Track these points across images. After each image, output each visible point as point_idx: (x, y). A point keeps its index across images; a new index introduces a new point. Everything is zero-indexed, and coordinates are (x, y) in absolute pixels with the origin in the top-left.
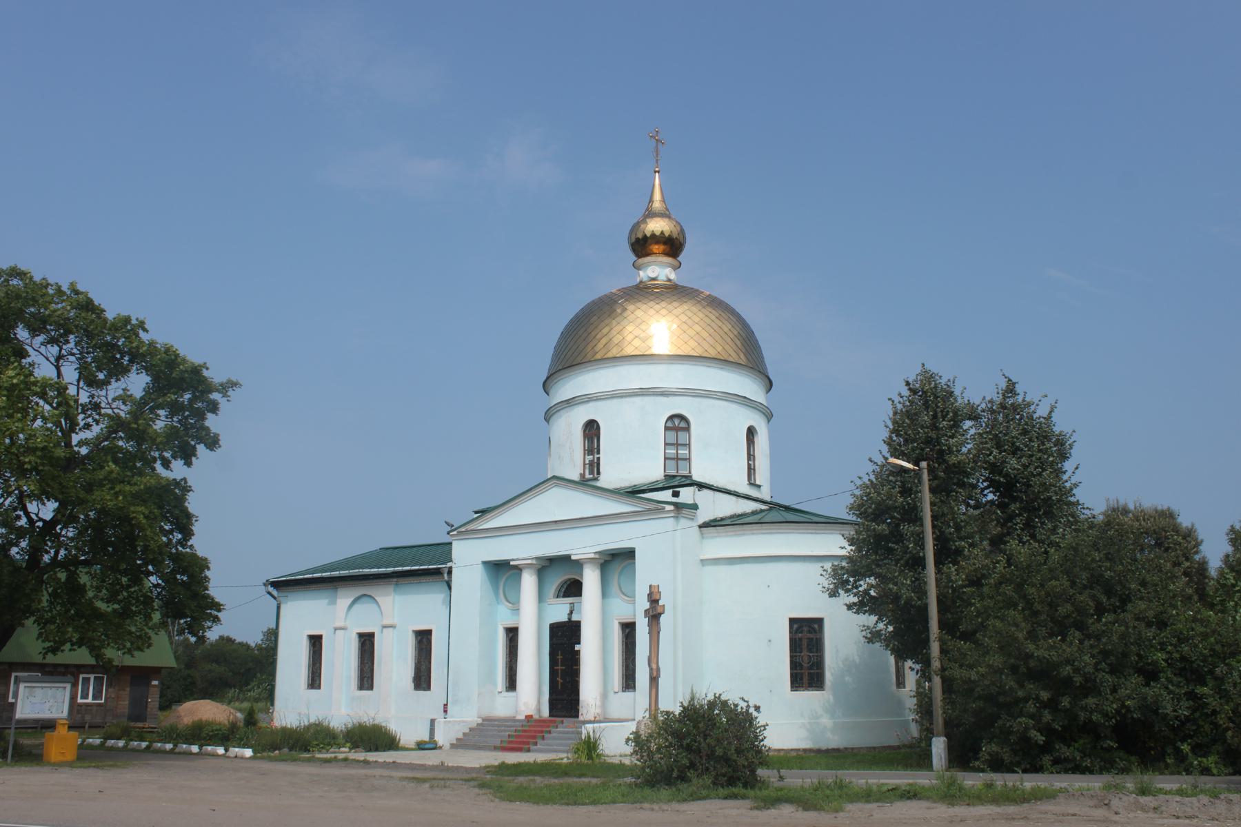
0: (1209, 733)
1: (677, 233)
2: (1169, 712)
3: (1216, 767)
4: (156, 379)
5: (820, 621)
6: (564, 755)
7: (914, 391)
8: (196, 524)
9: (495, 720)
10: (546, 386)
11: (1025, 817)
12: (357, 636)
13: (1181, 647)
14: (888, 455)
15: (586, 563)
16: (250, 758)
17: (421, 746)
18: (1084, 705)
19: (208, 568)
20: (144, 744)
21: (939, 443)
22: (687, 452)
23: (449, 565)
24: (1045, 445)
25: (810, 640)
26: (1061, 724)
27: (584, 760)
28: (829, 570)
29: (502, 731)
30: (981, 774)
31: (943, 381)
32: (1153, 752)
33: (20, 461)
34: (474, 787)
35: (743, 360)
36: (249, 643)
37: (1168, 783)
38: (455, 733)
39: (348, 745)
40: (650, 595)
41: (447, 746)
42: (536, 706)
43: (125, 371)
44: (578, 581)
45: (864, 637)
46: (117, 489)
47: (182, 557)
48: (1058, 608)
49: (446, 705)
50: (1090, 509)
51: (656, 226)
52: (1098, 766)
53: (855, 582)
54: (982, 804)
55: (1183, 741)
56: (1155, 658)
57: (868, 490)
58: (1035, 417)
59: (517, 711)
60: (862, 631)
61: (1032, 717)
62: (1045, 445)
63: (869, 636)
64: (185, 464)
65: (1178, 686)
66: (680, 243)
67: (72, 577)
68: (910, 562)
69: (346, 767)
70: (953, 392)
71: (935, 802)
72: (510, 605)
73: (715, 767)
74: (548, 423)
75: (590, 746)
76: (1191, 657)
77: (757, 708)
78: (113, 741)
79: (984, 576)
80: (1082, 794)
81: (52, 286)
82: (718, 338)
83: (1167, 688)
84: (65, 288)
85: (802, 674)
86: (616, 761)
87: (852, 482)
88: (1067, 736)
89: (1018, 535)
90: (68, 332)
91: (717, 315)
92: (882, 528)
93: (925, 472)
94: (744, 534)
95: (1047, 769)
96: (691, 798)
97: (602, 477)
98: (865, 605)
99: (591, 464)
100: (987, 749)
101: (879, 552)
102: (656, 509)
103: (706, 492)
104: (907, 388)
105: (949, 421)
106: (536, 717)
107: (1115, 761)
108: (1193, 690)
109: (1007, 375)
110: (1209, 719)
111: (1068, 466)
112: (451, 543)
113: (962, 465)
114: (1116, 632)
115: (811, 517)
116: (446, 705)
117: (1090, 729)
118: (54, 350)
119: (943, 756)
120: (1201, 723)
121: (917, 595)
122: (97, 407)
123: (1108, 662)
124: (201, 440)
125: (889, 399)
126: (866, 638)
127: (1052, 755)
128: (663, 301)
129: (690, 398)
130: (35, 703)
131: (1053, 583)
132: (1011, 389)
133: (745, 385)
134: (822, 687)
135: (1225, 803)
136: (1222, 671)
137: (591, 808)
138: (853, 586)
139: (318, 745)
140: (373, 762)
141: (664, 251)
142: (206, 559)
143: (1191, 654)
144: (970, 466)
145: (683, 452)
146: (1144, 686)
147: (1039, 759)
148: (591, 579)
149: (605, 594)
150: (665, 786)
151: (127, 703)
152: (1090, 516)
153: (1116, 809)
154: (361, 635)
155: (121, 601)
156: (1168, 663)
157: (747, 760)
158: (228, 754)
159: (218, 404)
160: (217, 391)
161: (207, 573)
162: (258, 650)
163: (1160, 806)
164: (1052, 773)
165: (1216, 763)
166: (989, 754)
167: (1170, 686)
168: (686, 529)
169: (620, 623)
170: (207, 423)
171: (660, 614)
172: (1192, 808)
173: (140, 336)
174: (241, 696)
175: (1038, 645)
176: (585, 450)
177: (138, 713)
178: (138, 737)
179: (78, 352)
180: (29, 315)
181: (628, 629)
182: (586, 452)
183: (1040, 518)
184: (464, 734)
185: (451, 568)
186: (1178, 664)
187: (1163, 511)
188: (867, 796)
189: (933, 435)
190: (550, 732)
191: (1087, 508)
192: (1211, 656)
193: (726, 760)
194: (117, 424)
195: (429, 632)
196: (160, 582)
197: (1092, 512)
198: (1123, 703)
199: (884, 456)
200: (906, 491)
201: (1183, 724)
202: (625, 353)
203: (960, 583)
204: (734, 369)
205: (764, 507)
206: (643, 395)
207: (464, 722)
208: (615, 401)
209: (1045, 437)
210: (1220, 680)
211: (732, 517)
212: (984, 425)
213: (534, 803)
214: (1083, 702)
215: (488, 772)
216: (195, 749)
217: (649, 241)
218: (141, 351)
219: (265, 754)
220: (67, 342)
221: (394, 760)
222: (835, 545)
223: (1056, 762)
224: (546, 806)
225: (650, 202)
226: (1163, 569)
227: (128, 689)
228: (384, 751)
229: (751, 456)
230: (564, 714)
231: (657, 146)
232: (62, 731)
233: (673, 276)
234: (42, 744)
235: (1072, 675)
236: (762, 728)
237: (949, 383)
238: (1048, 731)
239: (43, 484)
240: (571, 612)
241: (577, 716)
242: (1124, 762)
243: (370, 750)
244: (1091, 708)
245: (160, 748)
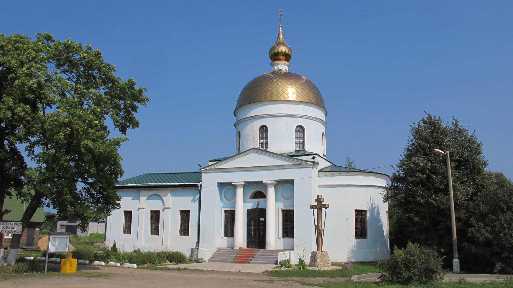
16: (137, 268)
41: (207, 261)
51: (283, 49)
103: (319, 157)
148: (271, 192)
169: (281, 210)
182: (260, 138)
185: (201, 184)
195: (188, 212)
240: (258, 205)
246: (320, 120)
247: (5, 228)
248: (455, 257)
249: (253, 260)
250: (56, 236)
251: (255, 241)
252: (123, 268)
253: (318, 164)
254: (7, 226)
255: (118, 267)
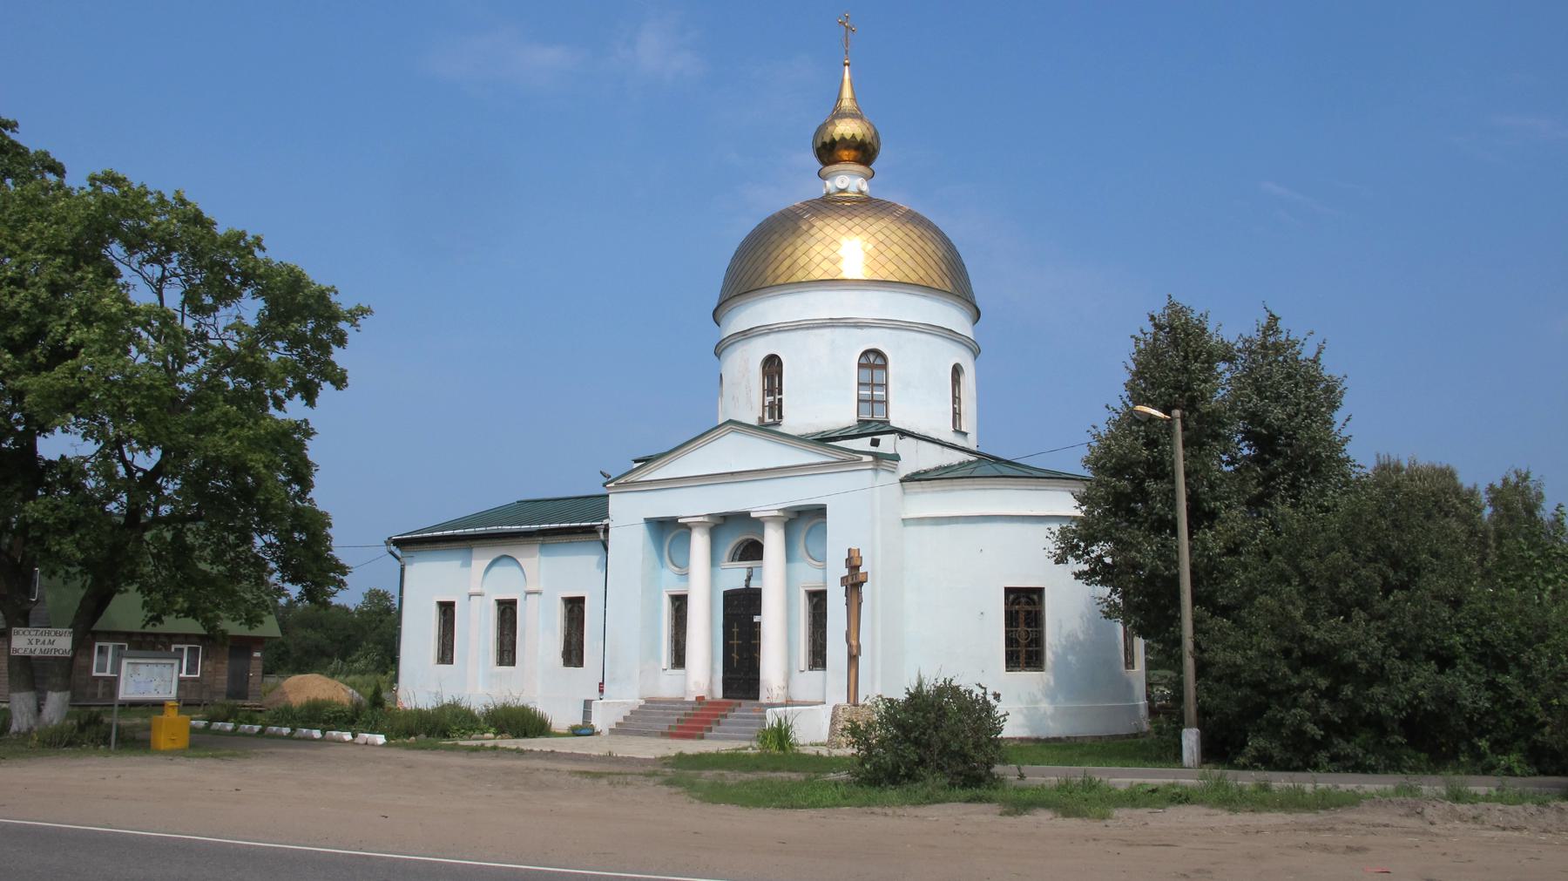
0: (1511, 727)
1: (870, 136)
2: (1468, 704)
3: (1519, 767)
4: (273, 303)
5: (1039, 592)
6: (746, 744)
7: (1158, 327)
8: (316, 474)
9: (660, 702)
10: (717, 316)
11: (1331, 828)
12: (496, 603)
13: (1482, 630)
14: (1131, 404)
15: (767, 521)
16: (383, 745)
17: (577, 732)
18: (1370, 696)
19: (330, 525)
20: (257, 728)
21: (1189, 389)
22: (884, 393)
23: (605, 522)
24: (1313, 392)
25: (1028, 613)
26: (1341, 715)
27: (774, 750)
28: (1057, 533)
29: (669, 714)
30: (1253, 774)
31: (1196, 315)
32: (1444, 749)
33: (122, 403)
34: (661, 784)
35: (949, 287)
36: (348, 606)
37: (1480, 786)
38: (616, 716)
39: (492, 730)
40: (848, 561)
41: (606, 731)
42: (709, 686)
43: (237, 295)
44: (758, 542)
45: (1101, 611)
46: (230, 434)
47: (302, 513)
48: (1341, 585)
49: (601, 684)
50: (1362, 467)
51: (846, 128)
52: (1383, 765)
53: (1086, 547)
54: (1269, 811)
55: (1481, 735)
56: (1452, 641)
57: (1108, 442)
58: (1299, 359)
59: (685, 692)
60: (1098, 604)
61: (1307, 708)
62: (1313, 392)
63: (1106, 609)
64: (306, 405)
65: (1478, 674)
66: (874, 148)
67: (179, 536)
68: (1156, 524)
69: (497, 757)
70: (1205, 329)
71: (1212, 807)
72: (677, 569)
73: (949, 764)
74: (719, 358)
75: (781, 735)
76: (1493, 641)
77: (997, 696)
78: (220, 724)
79: (1243, 543)
80: (1390, 801)
81: (152, 194)
82: (919, 259)
83: (1465, 676)
84: (169, 197)
85: (1018, 652)
86: (811, 751)
87: (1088, 431)
88: (1345, 730)
89: (1282, 497)
90: (170, 249)
91: (919, 234)
92: (1125, 485)
93: (1179, 421)
94: (953, 490)
95: (1324, 767)
96: (928, 801)
97: (784, 421)
98: (1097, 573)
99: (771, 406)
100: (1255, 743)
101: (1120, 513)
102: (853, 458)
103: (908, 440)
104: (1151, 323)
105: (1203, 363)
106: (708, 698)
107: (1402, 758)
108: (1494, 679)
109: (1268, 308)
110: (1512, 712)
111: (1338, 417)
112: (608, 496)
113: (1217, 414)
114: (1409, 612)
115: (1030, 471)
116: (601, 684)
117: (1376, 723)
118: (155, 271)
119: (1195, 750)
120: (1502, 716)
121: (1165, 564)
122: (203, 337)
123: (1400, 646)
124: (326, 377)
125: (1132, 337)
126: (1104, 612)
127: (1329, 751)
128: (856, 216)
129: (888, 331)
130: (140, 682)
131: (1333, 555)
132: (1272, 324)
133: (952, 316)
134: (1041, 667)
135: (1554, 812)
136: (1529, 658)
137: (812, 812)
138: (1083, 551)
139: (458, 730)
140: (527, 750)
141: (855, 156)
142: (326, 514)
143: (1493, 637)
144: (1227, 416)
145: (878, 393)
146: (1438, 674)
147: (1313, 756)
148: (773, 540)
149: (789, 556)
150: (890, 786)
151: (225, 677)
152: (1363, 475)
153: (1431, 819)
154: (500, 603)
155: (228, 563)
156: (1467, 649)
157: (986, 755)
158: (357, 740)
159: (346, 335)
160: (345, 319)
161: (329, 531)
162: (358, 614)
163: (1480, 815)
164: (1329, 771)
165: (1519, 761)
166: (1256, 749)
167: (1469, 675)
168: (888, 480)
170: (332, 358)
171: (861, 583)
172: (1518, 819)
173: (255, 254)
174: (345, 668)
175: (1316, 626)
176: (764, 390)
177: (239, 689)
178: (246, 718)
179: (183, 273)
180: (127, 228)
181: (818, 600)
183: (1306, 476)
184: (625, 718)
185: (607, 525)
186: (1478, 648)
187: (1441, 470)
188: (1133, 799)
189: (1184, 378)
190: (726, 716)
191: (1359, 466)
192: (1515, 639)
193: (964, 757)
194: (226, 359)
195: (581, 600)
196: (274, 541)
197: (1363, 470)
198: (1416, 692)
199: (1124, 402)
200: (1151, 443)
201: (1482, 716)
202: (812, 277)
203: (1218, 551)
204: (938, 297)
205: (972, 458)
206: (833, 326)
207: (624, 703)
208: (800, 333)
209: (1312, 383)
210: (1526, 668)
211: (936, 469)
212: (1240, 368)
213: (742, 806)
214: (1370, 692)
215: (665, 764)
216: (317, 734)
217: (838, 146)
218: (258, 272)
219: (399, 741)
220: (170, 261)
221: (553, 749)
222: (1064, 504)
223: (1334, 758)
224: (758, 809)
225: (838, 100)
226: (1459, 540)
227: (227, 662)
228: (534, 737)
229: (956, 399)
230: (740, 695)
231: (847, 32)
232: (172, 714)
233: (865, 188)
234: (148, 728)
235: (1357, 660)
236: (1002, 719)
237: (1201, 319)
238: (1325, 723)
239: (150, 430)
241: (757, 697)
242: (1413, 760)
243: (518, 736)
244: (1378, 699)
245: (275, 732)
246: (940, 330)
247: (34, 642)
248: (1186, 722)
249: (716, 731)
250: (138, 661)
251: (740, 679)
252: (294, 742)
253: (896, 458)
254: (37, 637)
255: (315, 740)
